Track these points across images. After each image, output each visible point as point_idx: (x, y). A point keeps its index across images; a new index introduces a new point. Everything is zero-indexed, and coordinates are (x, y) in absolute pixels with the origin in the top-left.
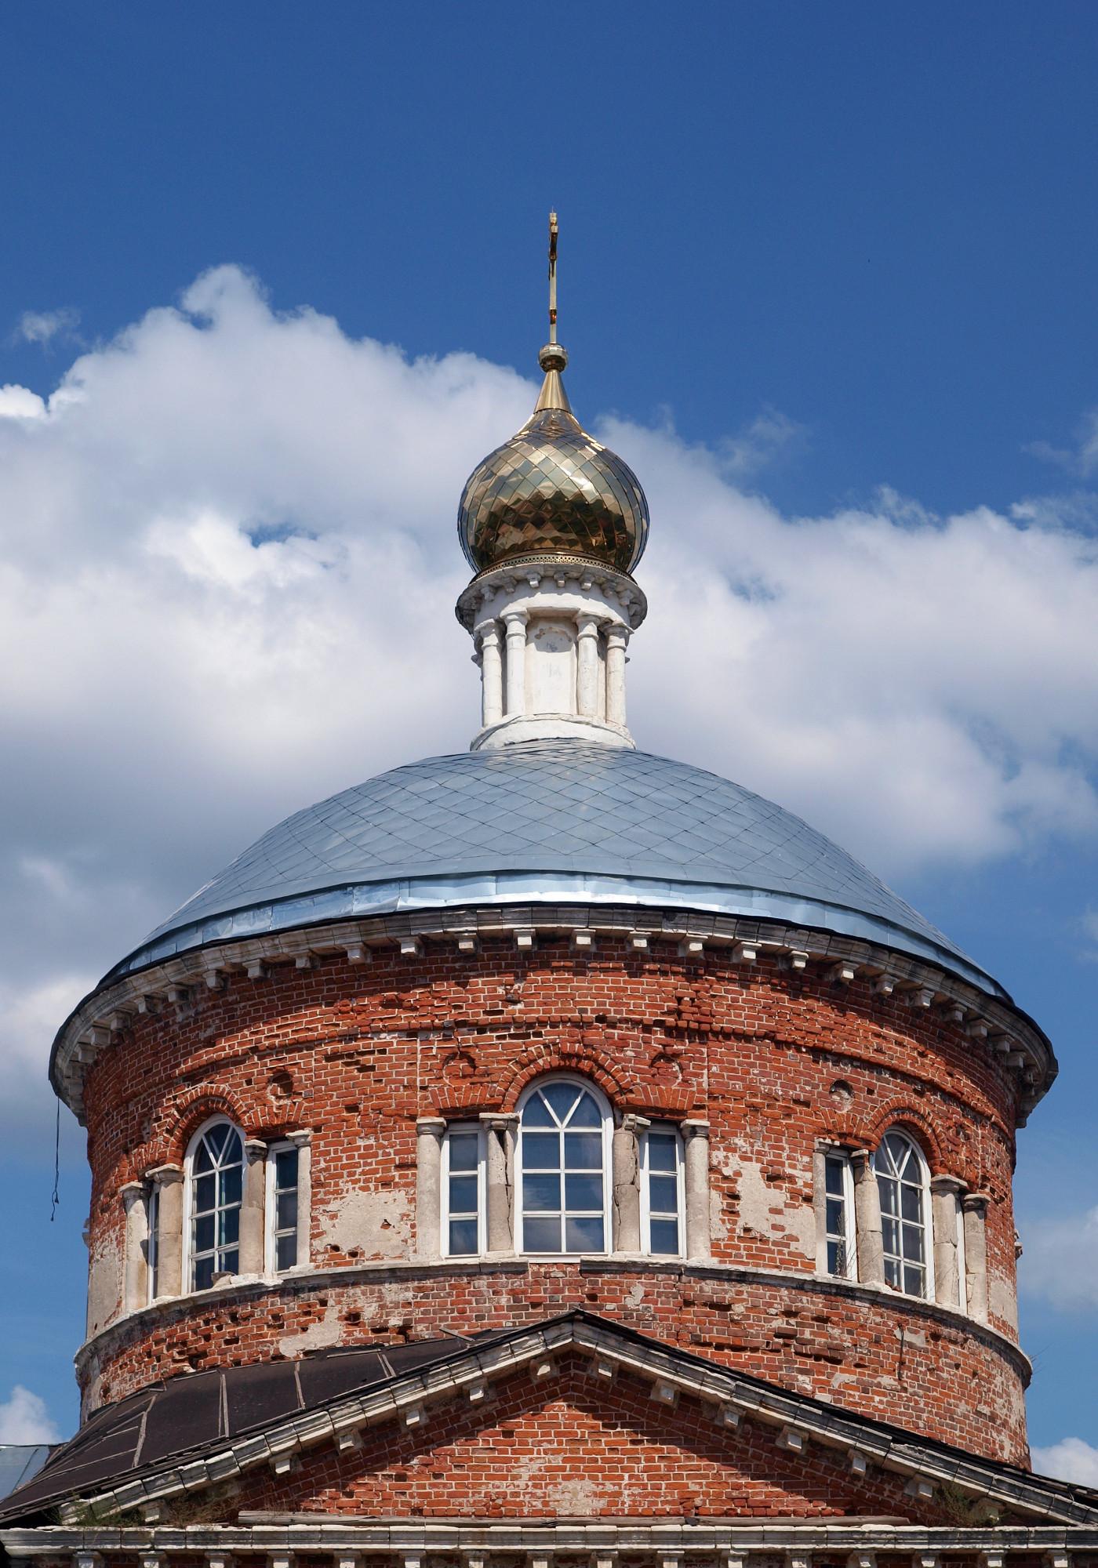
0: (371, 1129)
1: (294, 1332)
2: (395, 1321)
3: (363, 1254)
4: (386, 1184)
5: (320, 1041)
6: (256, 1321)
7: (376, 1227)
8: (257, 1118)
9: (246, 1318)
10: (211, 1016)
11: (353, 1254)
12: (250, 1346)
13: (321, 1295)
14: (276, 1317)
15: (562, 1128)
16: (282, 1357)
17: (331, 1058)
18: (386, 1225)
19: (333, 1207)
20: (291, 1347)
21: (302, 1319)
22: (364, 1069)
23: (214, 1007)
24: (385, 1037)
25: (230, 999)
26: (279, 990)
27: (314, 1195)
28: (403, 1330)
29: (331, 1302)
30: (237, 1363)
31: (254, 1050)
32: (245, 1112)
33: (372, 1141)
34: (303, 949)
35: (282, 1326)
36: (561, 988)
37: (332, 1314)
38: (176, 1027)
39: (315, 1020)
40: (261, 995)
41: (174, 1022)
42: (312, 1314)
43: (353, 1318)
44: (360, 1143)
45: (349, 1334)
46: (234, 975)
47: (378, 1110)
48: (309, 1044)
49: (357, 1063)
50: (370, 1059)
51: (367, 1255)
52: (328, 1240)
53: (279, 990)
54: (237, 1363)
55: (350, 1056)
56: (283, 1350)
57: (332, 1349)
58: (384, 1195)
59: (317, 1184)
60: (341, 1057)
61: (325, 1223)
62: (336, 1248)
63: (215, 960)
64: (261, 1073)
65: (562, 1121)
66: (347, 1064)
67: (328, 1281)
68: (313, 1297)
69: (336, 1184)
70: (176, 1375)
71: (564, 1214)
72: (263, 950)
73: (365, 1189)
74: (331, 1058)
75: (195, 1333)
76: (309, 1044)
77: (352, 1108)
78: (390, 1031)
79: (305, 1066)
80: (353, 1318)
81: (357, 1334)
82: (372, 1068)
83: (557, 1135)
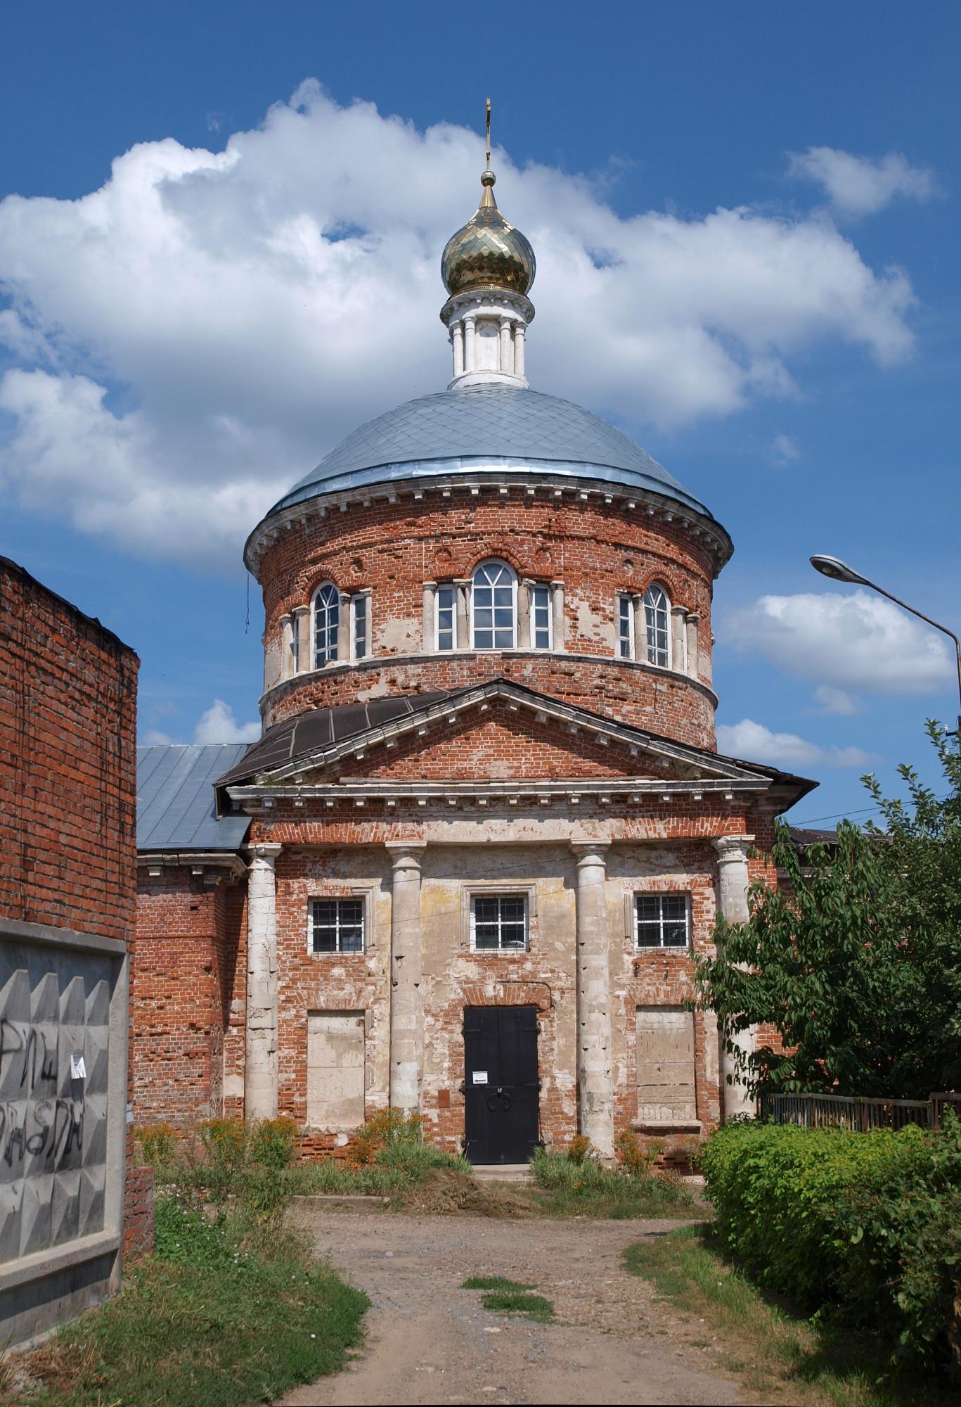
0: (401, 587)
2: (413, 684)
17: (380, 552)
18: (408, 636)
20: (363, 696)
22: (397, 557)
28: (417, 688)
34: (367, 497)
37: (383, 680)
39: (373, 532)
42: (373, 680)
43: (393, 682)
48: (371, 545)
52: (381, 643)
57: (383, 698)
58: (408, 621)
59: (375, 615)
61: (379, 635)
68: (373, 672)
71: (493, 608)
72: (348, 497)
76: (371, 545)
77: (392, 577)
79: (368, 555)
80: (393, 682)
81: (395, 690)
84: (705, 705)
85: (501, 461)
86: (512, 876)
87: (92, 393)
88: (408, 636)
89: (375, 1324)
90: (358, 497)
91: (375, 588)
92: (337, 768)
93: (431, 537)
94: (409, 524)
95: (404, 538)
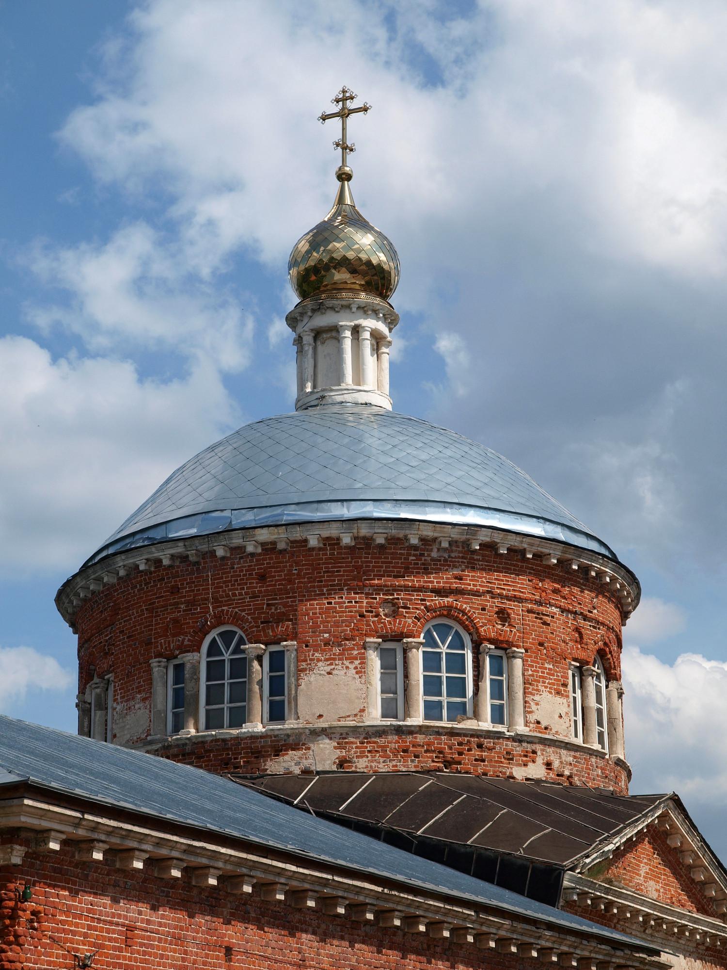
0: (552, 660)
1: (520, 765)
2: (567, 773)
3: (551, 730)
4: (558, 693)
5: (526, 600)
6: (496, 753)
7: (557, 716)
8: (489, 632)
9: (490, 749)
10: (458, 562)
11: (546, 728)
12: (495, 766)
13: (534, 747)
14: (508, 753)
15: (444, 650)
16: (514, 778)
17: (530, 611)
18: (561, 717)
19: (537, 698)
20: (519, 773)
21: (525, 759)
22: (545, 623)
23: (463, 558)
24: (554, 609)
25: (476, 557)
26: (506, 563)
27: (525, 688)
28: (570, 777)
29: (539, 753)
30: (485, 774)
31: (488, 592)
32: (482, 626)
33: (551, 667)
34: (534, 549)
35: (512, 759)
36: (434, 564)
37: (540, 760)
38: (429, 559)
39: (522, 584)
40: (495, 562)
41: (429, 555)
42: (530, 757)
43: (548, 765)
44: (546, 665)
45: (548, 774)
46: (490, 547)
47: (553, 649)
48: (520, 600)
49: (541, 619)
50: (548, 619)
51: (553, 731)
53: (506, 563)
54: (485, 774)
55: (538, 614)
56: (515, 774)
58: (559, 699)
59: (526, 682)
60: (534, 613)
61: (534, 707)
62: (538, 722)
63: (487, 536)
64: (491, 607)
65: (443, 643)
66: (536, 618)
67: (537, 741)
68: (529, 747)
69: (537, 686)
70: (436, 770)
73: (551, 693)
74: (530, 611)
75: (450, 748)
76: (520, 600)
77: (541, 644)
78: (556, 607)
79: (516, 610)
82: (549, 625)
83: (440, 653)
84: (623, 776)
85: (464, 510)
86: (439, 819)
87: (126, 372)
88: (561, 717)
89: (67, 558)
90: (497, 537)
91: (526, 651)
92: (580, 910)
93: (571, 612)
94: (556, 591)
95: (551, 605)
